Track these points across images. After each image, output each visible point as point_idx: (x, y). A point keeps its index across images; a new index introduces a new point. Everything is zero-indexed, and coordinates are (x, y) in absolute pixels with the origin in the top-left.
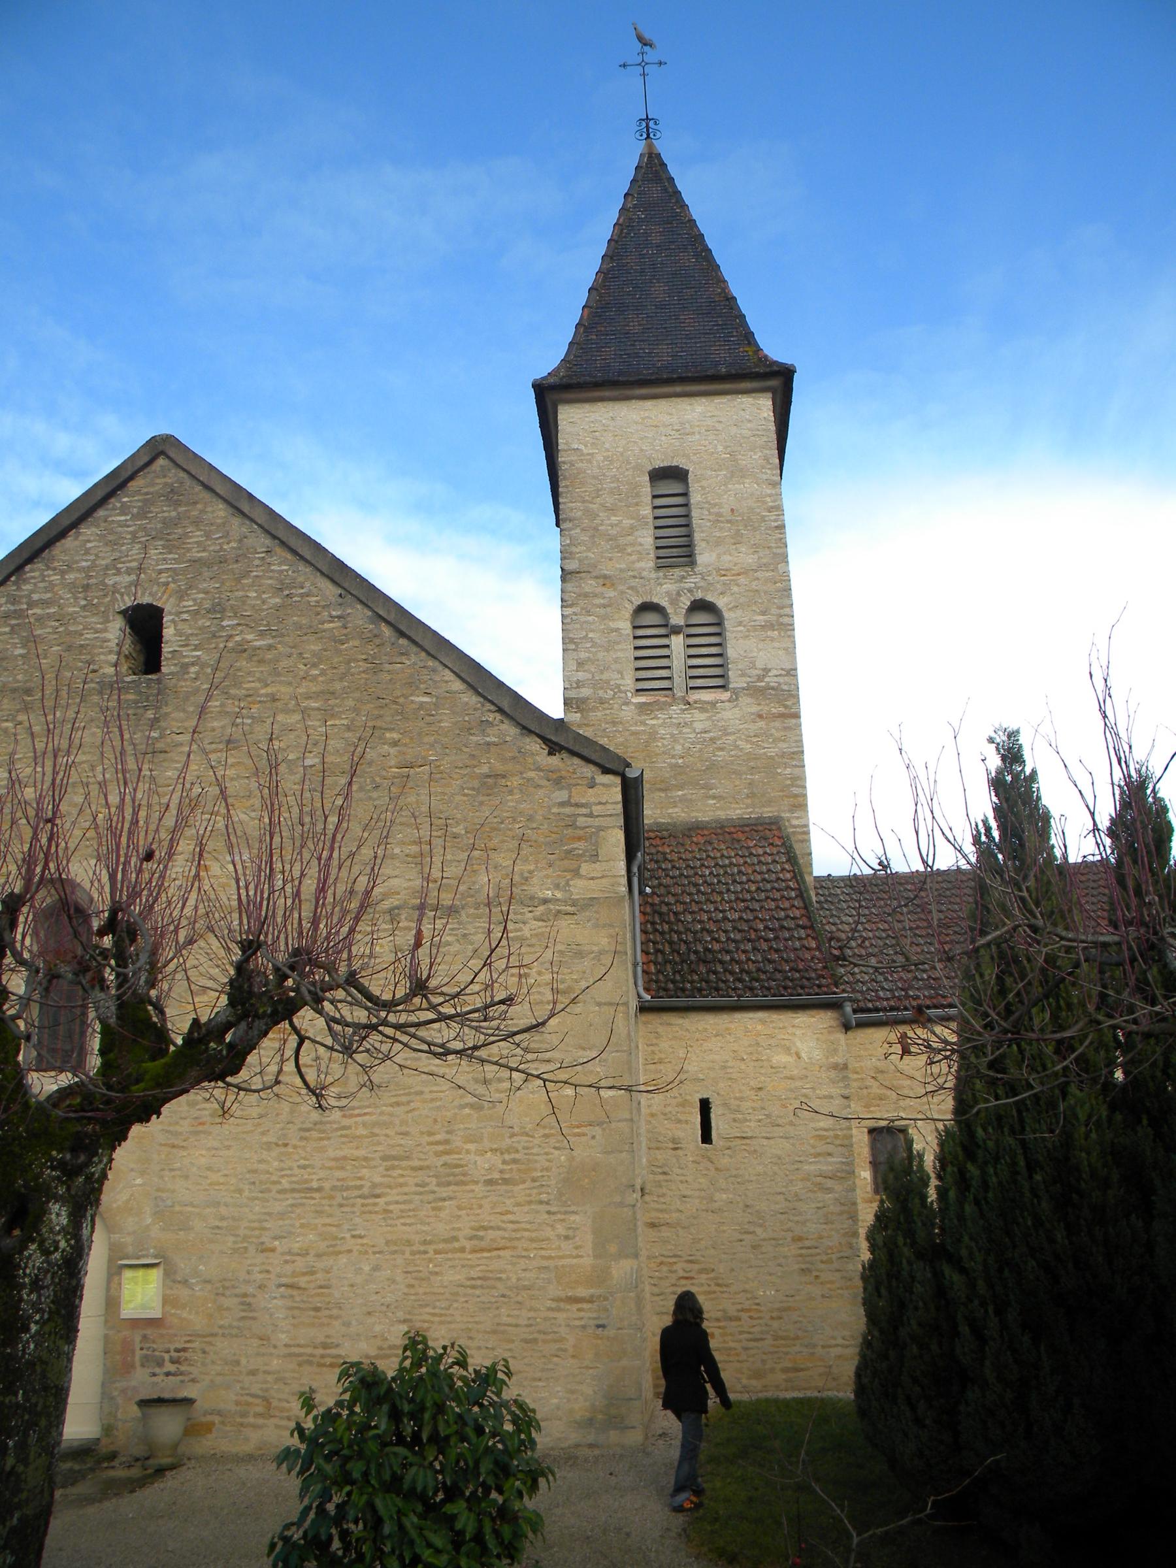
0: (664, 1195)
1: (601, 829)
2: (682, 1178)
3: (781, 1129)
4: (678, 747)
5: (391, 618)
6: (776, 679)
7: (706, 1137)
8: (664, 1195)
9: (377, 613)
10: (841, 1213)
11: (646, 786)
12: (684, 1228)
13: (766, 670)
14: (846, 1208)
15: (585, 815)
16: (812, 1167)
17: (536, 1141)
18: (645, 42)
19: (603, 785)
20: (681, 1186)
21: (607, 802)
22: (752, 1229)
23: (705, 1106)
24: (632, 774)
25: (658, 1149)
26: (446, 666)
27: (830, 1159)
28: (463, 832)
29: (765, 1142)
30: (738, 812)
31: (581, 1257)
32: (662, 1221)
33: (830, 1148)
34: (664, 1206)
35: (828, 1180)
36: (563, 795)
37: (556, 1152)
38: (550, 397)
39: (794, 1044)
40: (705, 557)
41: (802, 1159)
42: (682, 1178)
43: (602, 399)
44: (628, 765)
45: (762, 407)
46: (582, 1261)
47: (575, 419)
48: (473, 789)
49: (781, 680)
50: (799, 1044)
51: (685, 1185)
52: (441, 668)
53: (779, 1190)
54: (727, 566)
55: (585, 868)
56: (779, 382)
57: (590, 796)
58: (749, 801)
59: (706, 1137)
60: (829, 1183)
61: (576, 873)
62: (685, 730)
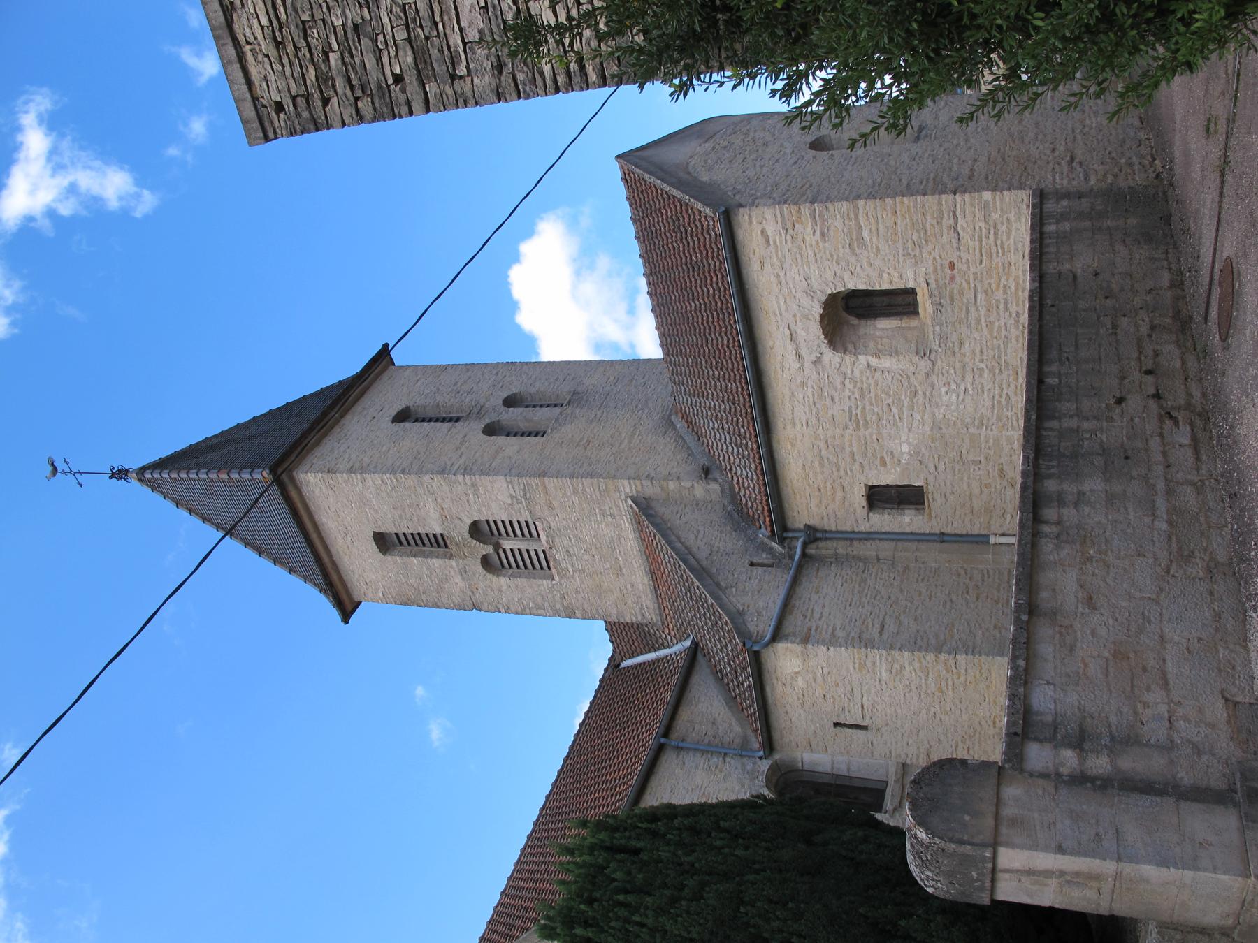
4: (586, 557)
13: (512, 497)
23: (836, 725)
60: (896, 666)
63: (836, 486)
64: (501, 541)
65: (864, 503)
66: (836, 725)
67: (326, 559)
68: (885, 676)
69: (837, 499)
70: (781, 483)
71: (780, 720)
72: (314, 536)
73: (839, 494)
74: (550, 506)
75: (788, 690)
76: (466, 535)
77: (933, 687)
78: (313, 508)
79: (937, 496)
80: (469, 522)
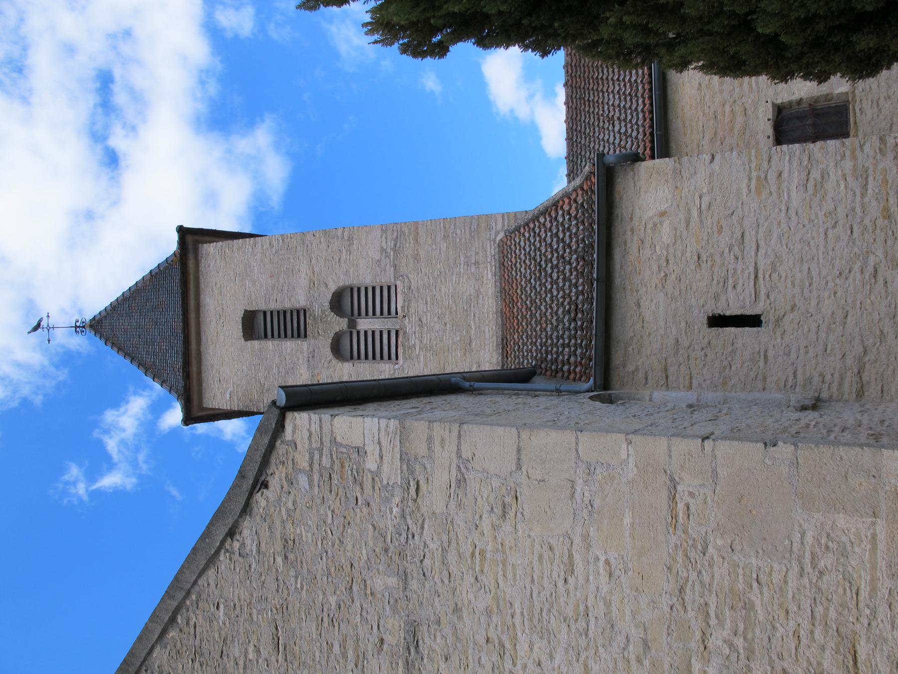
0: (822, 375)
1: (334, 441)
2: (802, 351)
3: (747, 234)
4: (437, 327)
5: (159, 629)
6: (389, 243)
7: (754, 321)
8: (822, 375)
9: (156, 641)
10: (854, 157)
11: (290, 382)
12: (865, 352)
13: (383, 250)
14: (848, 153)
15: (321, 456)
16: (794, 194)
17: (693, 576)
18: (38, 326)
19: (294, 432)
20: (811, 354)
21: (309, 430)
22: (870, 269)
23: (717, 321)
24: (282, 400)
25: (765, 379)
26: (195, 582)
27: (785, 175)
28: (335, 598)
29: (762, 251)
30: (490, 275)
31: (874, 537)
32: (855, 379)
33: (772, 176)
34: (836, 375)
35: (812, 177)
36: (303, 480)
37: (711, 550)
38: (196, 413)
39: (650, 218)
40: (300, 300)
41: (784, 208)
42: (802, 351)
43: (199, 373)
44: (274, 403)
45: (210, 250)
46: (882, 536)
47: (217, 395)
48: (296, 577)
49: (389, 238)
50: (650, 213)
51: (811, 349)
52: (197, 588)
53: (822, 236)
54: (307, 282)
55: (371, 464)
56: (191, 239)
57: (303, 445)
58: (481, 266)
59: (754, 321)
60: (815, 174)
61: (376, 475)
62: (424, 321)
63: (737, 108)
64: (358, 320)
65: (770, 131)
66: (717, 321)
67: (193, 345)
68: (796, 198)
69: (737, 127)
70: (671, 114)
71: (627, 326)
72: (192, 315)
73: (740, 119)
74: (416, 258)
75: (647, 252)
76: (327, 304)
77: (874, 210)
78: (202, 285)
79: (866, 105)
80: (333, 288)
